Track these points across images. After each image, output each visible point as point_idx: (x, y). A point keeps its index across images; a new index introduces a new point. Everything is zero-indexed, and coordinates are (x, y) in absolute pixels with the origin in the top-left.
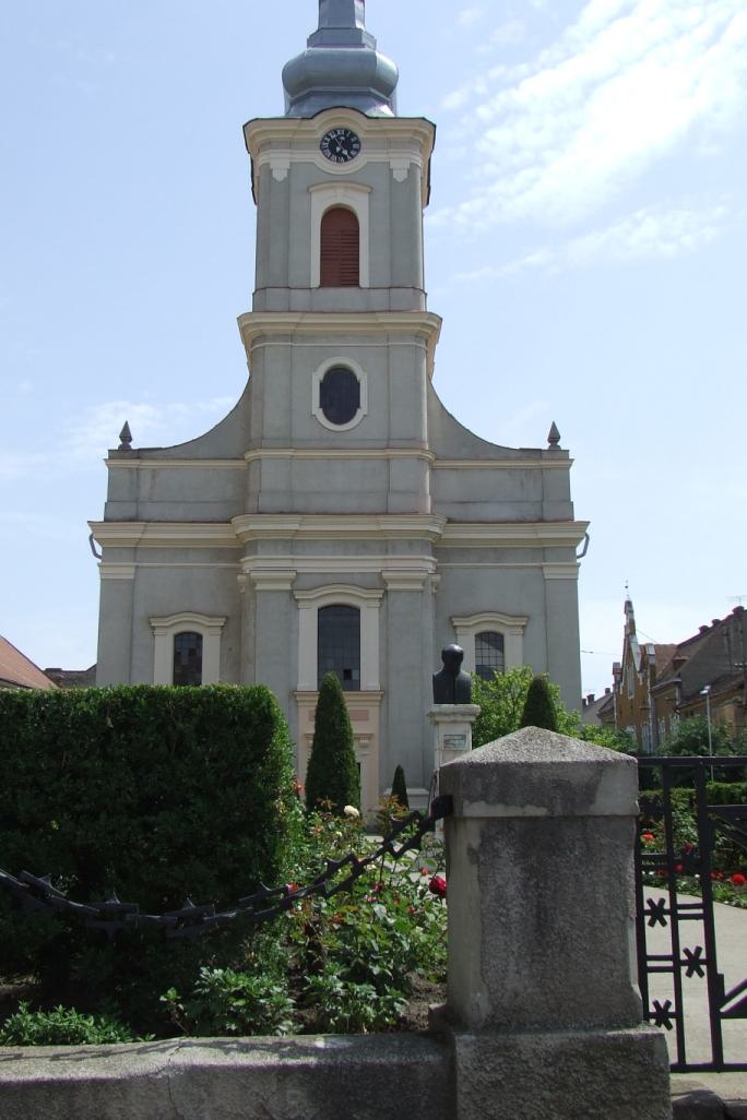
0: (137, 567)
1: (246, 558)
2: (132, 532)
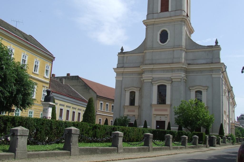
0: (123, 77)
1: (143, 75)
2: (121, 70)
